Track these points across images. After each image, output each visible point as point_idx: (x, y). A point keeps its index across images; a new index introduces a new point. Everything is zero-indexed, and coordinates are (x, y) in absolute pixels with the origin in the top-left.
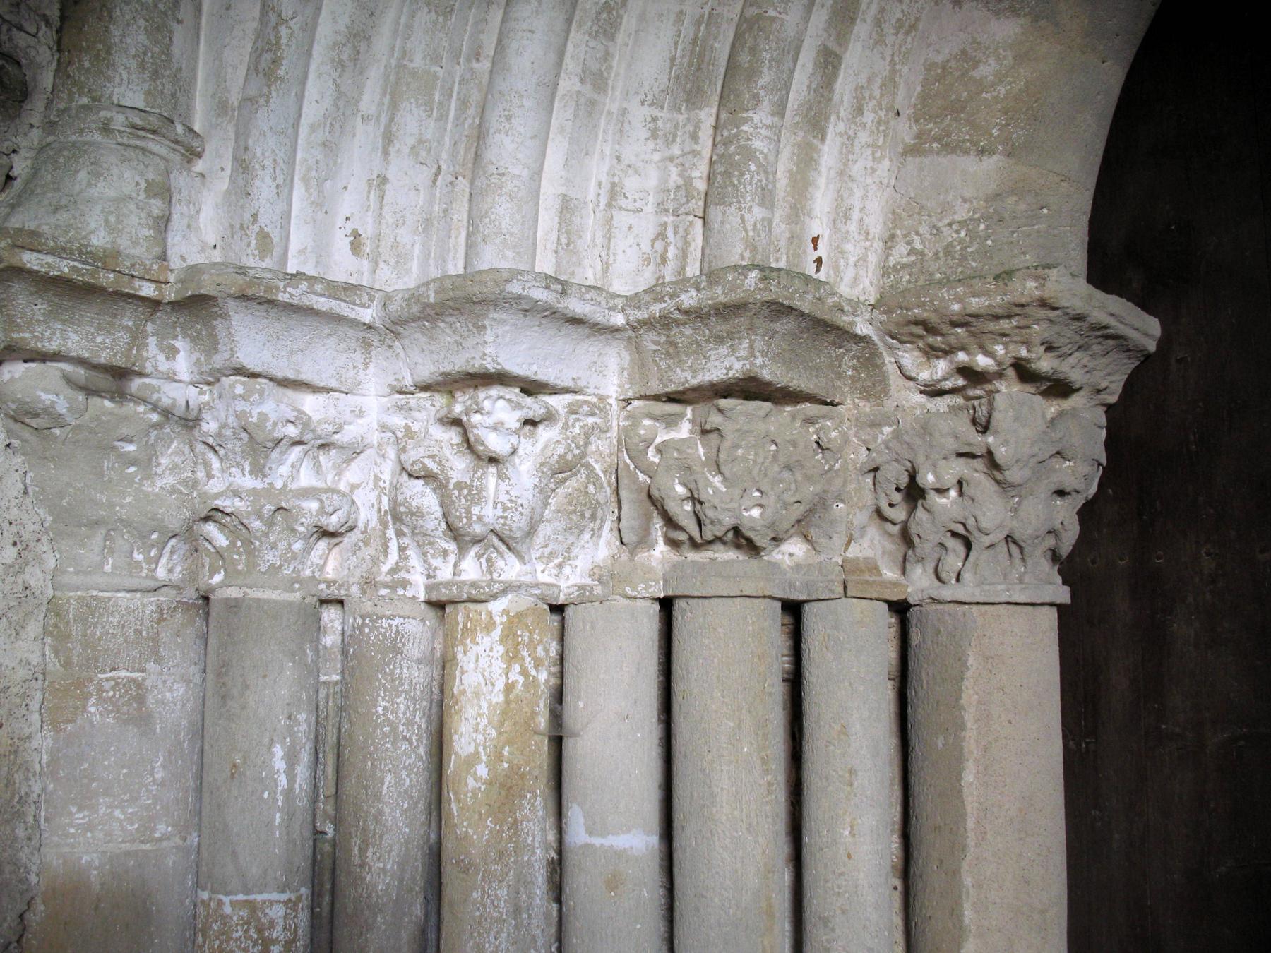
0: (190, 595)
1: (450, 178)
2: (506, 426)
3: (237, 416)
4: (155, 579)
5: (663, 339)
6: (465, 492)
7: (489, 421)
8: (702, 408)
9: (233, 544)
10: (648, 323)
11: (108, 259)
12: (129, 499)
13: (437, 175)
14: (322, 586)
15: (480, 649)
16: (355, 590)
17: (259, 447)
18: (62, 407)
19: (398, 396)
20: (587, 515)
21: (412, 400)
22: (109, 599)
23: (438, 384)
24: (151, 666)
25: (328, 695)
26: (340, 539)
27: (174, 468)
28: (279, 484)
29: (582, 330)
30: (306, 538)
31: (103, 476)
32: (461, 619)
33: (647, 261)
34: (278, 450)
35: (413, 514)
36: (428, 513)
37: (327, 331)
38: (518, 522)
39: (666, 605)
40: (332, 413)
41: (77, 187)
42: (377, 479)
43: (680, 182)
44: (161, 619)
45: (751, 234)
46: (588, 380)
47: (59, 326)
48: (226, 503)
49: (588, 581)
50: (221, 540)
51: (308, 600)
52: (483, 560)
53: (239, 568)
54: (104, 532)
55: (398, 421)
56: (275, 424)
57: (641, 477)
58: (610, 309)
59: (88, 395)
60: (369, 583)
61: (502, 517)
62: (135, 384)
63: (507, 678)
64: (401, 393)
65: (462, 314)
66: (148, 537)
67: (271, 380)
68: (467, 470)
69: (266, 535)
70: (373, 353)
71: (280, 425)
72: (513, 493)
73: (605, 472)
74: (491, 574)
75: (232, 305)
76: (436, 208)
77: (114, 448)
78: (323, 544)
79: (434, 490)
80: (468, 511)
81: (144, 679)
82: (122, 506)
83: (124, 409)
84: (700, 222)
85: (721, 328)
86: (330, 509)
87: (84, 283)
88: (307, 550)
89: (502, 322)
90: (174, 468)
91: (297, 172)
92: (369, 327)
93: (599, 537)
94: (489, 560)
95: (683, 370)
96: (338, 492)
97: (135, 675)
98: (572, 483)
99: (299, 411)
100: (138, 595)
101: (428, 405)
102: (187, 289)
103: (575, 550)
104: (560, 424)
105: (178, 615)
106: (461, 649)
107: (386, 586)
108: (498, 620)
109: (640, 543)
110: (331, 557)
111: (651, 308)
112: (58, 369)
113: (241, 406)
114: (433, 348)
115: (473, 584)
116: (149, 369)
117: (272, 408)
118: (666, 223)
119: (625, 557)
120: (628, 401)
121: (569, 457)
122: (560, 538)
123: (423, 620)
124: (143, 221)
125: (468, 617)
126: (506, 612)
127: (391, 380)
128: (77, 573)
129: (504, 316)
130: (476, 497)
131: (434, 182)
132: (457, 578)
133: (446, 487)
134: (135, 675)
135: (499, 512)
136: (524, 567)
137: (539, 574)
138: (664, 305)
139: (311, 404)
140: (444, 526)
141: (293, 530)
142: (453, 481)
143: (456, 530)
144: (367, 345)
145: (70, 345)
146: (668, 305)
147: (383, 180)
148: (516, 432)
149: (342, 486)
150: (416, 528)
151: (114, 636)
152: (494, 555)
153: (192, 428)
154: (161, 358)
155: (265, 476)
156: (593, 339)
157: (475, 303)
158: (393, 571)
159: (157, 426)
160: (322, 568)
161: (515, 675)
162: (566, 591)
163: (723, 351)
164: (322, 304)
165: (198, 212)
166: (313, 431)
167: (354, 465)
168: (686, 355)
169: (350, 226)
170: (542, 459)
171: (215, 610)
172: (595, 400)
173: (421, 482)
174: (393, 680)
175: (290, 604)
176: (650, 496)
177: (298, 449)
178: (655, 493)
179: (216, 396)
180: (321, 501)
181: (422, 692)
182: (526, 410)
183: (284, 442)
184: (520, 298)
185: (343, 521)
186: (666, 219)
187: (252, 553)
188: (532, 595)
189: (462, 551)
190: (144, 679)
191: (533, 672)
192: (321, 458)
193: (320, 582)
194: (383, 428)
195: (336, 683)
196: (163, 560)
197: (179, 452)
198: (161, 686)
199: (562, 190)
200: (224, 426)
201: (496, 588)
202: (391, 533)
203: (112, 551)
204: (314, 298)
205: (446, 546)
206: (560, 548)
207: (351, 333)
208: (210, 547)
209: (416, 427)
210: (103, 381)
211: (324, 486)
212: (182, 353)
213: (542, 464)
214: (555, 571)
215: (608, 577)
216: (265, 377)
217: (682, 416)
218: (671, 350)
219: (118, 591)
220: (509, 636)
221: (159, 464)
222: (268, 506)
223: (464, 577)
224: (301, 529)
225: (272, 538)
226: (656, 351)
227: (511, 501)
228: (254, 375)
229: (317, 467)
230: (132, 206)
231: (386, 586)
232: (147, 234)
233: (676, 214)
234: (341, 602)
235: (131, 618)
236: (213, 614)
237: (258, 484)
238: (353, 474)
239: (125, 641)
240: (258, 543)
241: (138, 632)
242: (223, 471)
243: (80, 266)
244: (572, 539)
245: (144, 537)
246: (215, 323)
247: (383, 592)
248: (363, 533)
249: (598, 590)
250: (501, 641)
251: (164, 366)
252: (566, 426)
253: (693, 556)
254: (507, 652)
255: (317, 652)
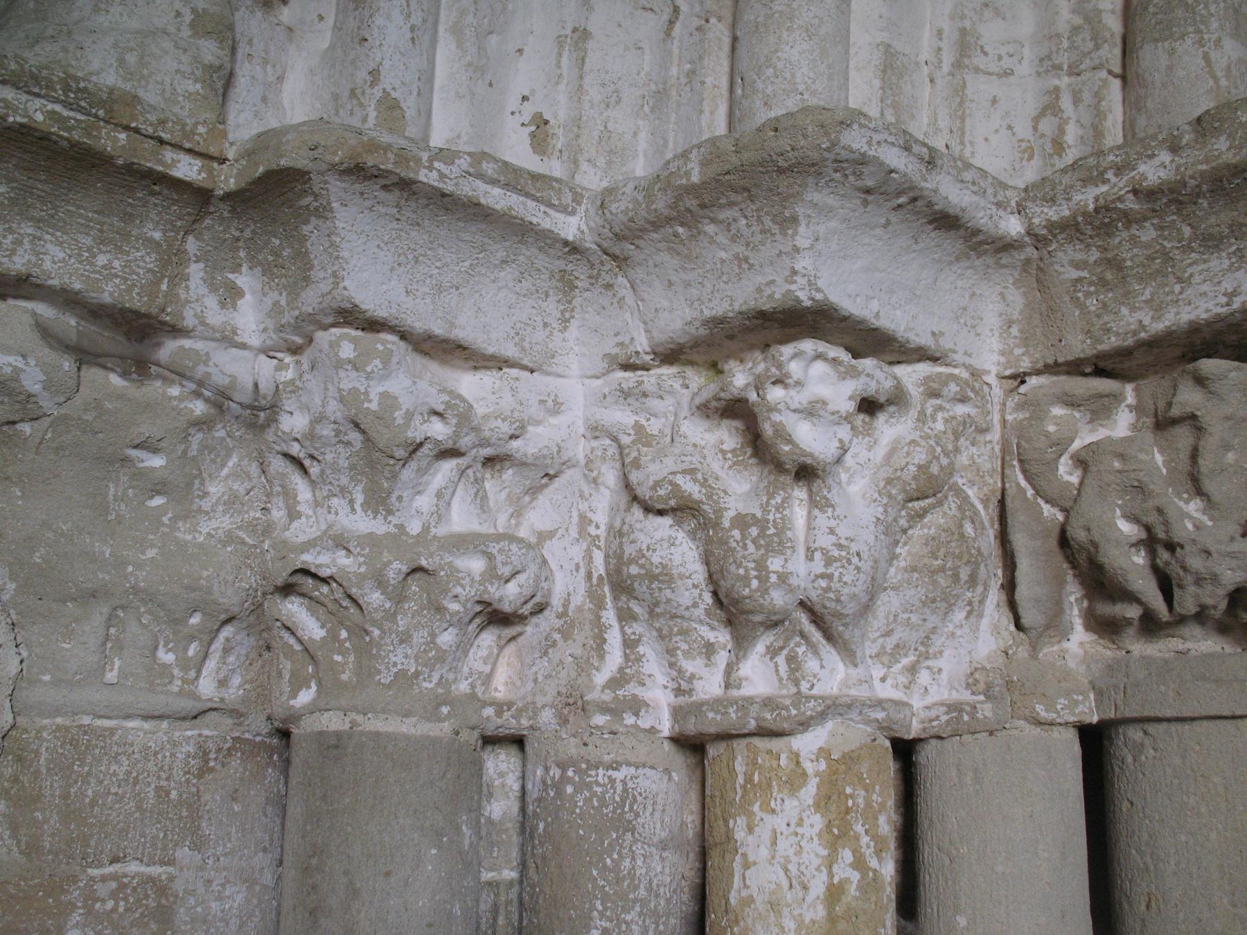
0: (256, 727)
1: (696, 22)
2: (831, 407)
3: (342, 400)
4: (196, 697)
5: (1095, 255)
6: (754, 531)
7: (799, 398)
8: (1155, 386)
9: (333, 636)
10: (1069, 228)
11: (116, 108)
12: (151, 553)
13: (671, 23)
14: (489, 711)
15: (778, 822)
16: (547, 716)
17: (381, 456)
18: (32, 381)
19: (621, 374)
20: (964, 576)
21: (649, 379)
22: (112, 731)
23: (696, 344)
24: (184, 853)
25: (495, 909)
26: (518, 629)
27: (232, 502)
28: (414, 528)
29: (952, 244)
30: (460, 623)
31: (107, 513)
32: (740, 767)
33: (1029, 153)
34: (413, 465)
35: (653, 577)
36: (681, 576)
37: (501, 254)
38: (851, 583)
39: (1095, 740)
40: (507, 402)
41: (76, 15)
42: (584, 521)
43: (1078, 21)
44: (204, 770)
45: (1224, 82)
46: (954, 340)
47: (28, 229)
48: (322, 560)
49: (966, 696)
50: (313, 628)
51: (465, 735)
52: (781, 660)
53: (344, 677)
54: (106, 610)
55: (622, 417)
56: (409, 415)
57: (1047, 509)
58: (999, 205)
59: (80, 364)
60: (574, 705)
61: (823, 576)
62: (168, 349)
63: (831, 875)
64: (627, 367)
65: (752, 199)
66: (183, 621)
67: (404, 336)
68: (755, 491)
69: (392, 616)
70: (577, 302)
71: (417, 420)
72: (843, 531)
73: (985, 502)
74: (797, 684)
75: (336, 187)
76: (674, 71)
77: (125, 460)
78: (488, 638)
79: (692, 535)
80: (761, 566)
81: (171, 879)
82: (139, 566)
83: (144, 389)
84: (1116, 84)
85: (1217, 219)
86: (506, 571)
87: (74, 145)
88: (463, 647)
89: (826, 212)
90: (232, 502)
91: (443, 18)
92: (573, 249)
93: (981, 616)
94: (791, 659)
95: (1133, 309)
96: (520, 541)
97: (155, 870)
98: (936, 519)
99: (451, 393)
100: (165, 725)
101: (677, 385)
102: (257, 165)
103: (938, 641)
104: (913, 413)
105: (235, 763)
106: (741, 821)
107: (604, 709)
108: (809, 767)
109: (1048, 627)
110: (503, 661)
111: (1078, 197)
112: (26, 311)
113: (349, 380)
114: (690, 276)
115: (768, 702)
116: (189, 321)
117: (406, 388)
118: (1057, 90)
119: (1022, 652)
120: (1021, 378)
121: (935, 469)
122: (914, 618)
123: (667, 771)
124: (186, 68)
125: (755, 763)
126: (824, 753)
127: (610, 347)
128: (56, 683)
129: (831, 201)
130: (776, 542)
131: (668, 33)
132: (735, 693)
133: (716, 525)
134: (155, 870)
135: (818, 566)
136: (854, 672)
137: (877, 684)
138: (1104, 188)
139: (472, 385)
140: (708, 598)
141: (440, 609)
142: (730, 514)
143: (736, 602)
144: (567, 286)
145: (48, 265)
146: (1114, 186)
147: (582, 35)
148: (848, 418)
149: (523, 533)
150: (657, 604)
151: (120, 798)
152: (801, 650)
153: (264, 427)
154: (211, 302)
155: (390, 512)
156: (966, 264)
157: (781, 171)
158: (617, 682)
159: (202, 424)
160: (488, 679)
161: (844, 871)
162: (923, 715)
163: (1218, 263)
164: (496, 198)
165: (281, 79)
166: (476, 429)
167: (542, 499)
168: (1140, 280)
169: (529, 110)
170: (886, 472)
171: (300, 753)
172: (965, 375)
173: (667, 521)
174: (619, 881)
175: (434, 741)
176: (1064, 541)
177: (448, 467)
178: (1078, 534)
179: (306, 367)
180: (490, 557)
181: (668, 901)
182: (863, 379)
183: (425, 450)
184: (862, 161)
185: (527, 592)
186: (1056, 82)
187: (366, 651)
188: (867, 722)
189: (741, 643)
190: (171, 879)
191: (874, 863)
192: (487, 485)
193: (485, 704)
194: (596, 430)
195: (511, 883)
196: (211, 664)
197: (237, 475)
198: (201, 890)
199: (883, 37)
200: (319, 419)
201: (810, 708)
202: (609, 616)
203: (120, 647)
204: (481, 186)
205: (711, 636)
206: (913, 637)
207: (541, 261)
208: (292, 641)
209: (654, 426)
210: (103, 337)
211: (492, 531)
212: (248, 297)
213: (889, 481)
214: (902, 679)
215: (1006, 688)
216: (392, 329)
217: (1117, 398)
218: (1109, 276)
219: (128, 717)
220: (829, 798)
221: (206, 494)
222: (396, 565)
223: (747, 691)
224: (454, 607)
225: (402, 622)
226: (1079, 280)
227: (840, 547)
228: (374, 326)
229: (481, 498)
230: (167, 44)
231: (604, 709)
232: (191, 88)
233: (1074, 72)
234: (518, 742)
235: (151, 766)
236: (296, 761)
237: (379, 527)
238: (539, 517)
239: (139, 808)
240: (376, 633)
241: (162, 793)
242: (317, 504)
243: (66, 113)
244: (933, 620)
245: (176, 622)
246: (306, 229)
247: (600, 720)
248: (559, 616)
249: (986, 711)
250: (817, 806)
251: (215, 316)
252: (922, 418)
253: (1140, 648)
254: (829, 826)
255: (477, 827)
